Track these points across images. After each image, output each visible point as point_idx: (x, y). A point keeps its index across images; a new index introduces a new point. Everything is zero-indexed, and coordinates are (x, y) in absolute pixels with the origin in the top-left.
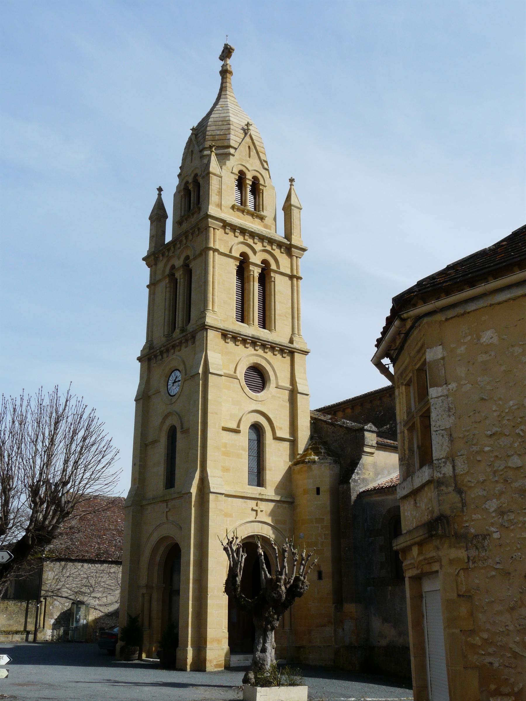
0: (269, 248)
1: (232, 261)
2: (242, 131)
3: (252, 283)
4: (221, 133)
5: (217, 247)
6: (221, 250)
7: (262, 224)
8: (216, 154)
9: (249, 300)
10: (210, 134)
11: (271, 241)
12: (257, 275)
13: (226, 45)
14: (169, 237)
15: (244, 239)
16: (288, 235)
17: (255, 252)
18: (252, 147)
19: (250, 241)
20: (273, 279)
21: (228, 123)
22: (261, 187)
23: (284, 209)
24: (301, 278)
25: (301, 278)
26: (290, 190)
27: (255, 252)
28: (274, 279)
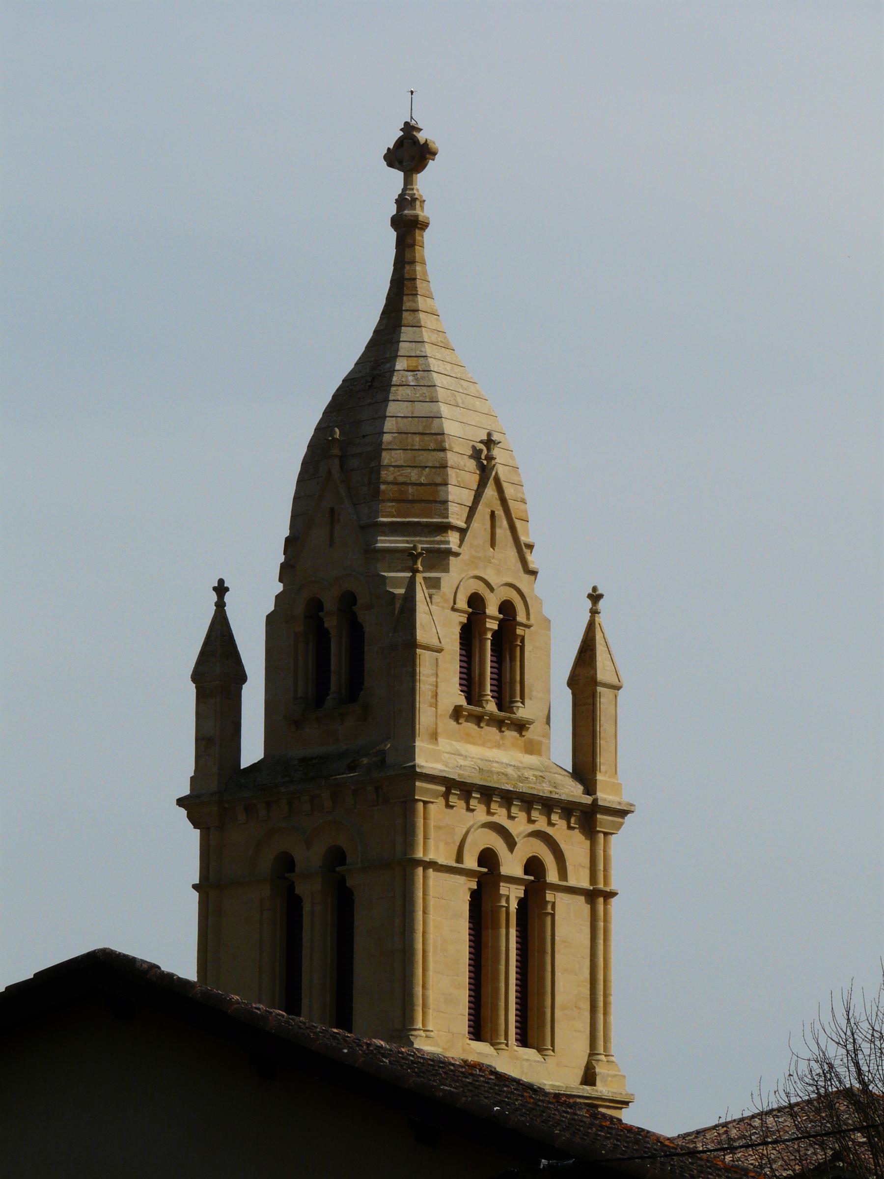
0: (541, 824)
1: (461, 880)
2: (472, 464)
3: (503, 931)
4: (423, 480)
5: (431, 856)
6: (442, 861)
7: (521, 741)
8: (425, 578)
9: (496, 978)
10: (390, 478)
11: (548, 805)
12: (514, 906)
13: (409, 129)
14: (252, 749)
15: (489, 813)
16: (584, 770)
17: (511, 844)
18: (500, 512)
19: (500, 816)
20: (549, 910)
21: (436, 441)
22: (519, 631)
23: (572, 682)
24: (613, 894)
25: (613, 894)
26: (591, 627)
27: (511, 844)
28: (553, 908)
